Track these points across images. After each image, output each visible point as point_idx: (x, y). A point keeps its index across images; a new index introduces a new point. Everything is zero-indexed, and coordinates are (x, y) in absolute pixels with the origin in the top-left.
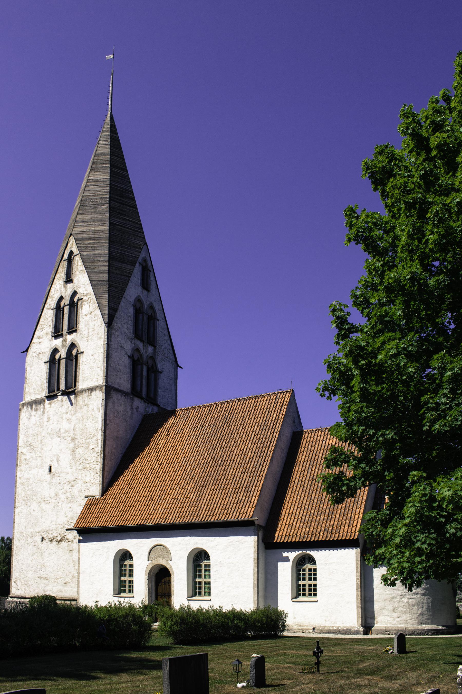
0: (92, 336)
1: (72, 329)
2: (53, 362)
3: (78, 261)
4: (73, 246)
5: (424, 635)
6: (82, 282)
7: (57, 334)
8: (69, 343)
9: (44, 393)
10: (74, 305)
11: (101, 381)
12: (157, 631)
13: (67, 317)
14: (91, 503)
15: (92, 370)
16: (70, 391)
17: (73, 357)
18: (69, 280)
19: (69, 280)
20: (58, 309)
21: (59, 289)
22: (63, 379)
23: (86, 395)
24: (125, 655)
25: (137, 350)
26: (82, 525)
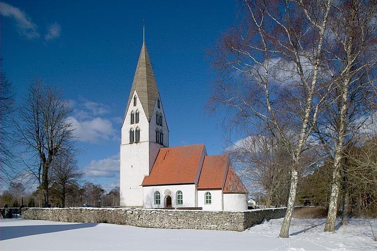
0: (144, 125)
1: (137, 122)
2: (131, 133)
3: (138, 99)
4: (135, 93)
5: (71, 222)
6: (139, 107)
7: (132, 123)
8: (136, 127)
9: (129, 142)
10: (137, 114)
11: (148, 139)
12: (348, 109)
13: (135, 118)
14: (146, 177)
15: (145, 135)
16: (138, 141)
17: (138, 132)
18: (135, 105)
19: (135, 105)
20: (132, 115)
21: (131, 108)
22: (135, 137)
23: (143, 143)
24: (144, 44)
25: (157, 128)
26: (144, 184)
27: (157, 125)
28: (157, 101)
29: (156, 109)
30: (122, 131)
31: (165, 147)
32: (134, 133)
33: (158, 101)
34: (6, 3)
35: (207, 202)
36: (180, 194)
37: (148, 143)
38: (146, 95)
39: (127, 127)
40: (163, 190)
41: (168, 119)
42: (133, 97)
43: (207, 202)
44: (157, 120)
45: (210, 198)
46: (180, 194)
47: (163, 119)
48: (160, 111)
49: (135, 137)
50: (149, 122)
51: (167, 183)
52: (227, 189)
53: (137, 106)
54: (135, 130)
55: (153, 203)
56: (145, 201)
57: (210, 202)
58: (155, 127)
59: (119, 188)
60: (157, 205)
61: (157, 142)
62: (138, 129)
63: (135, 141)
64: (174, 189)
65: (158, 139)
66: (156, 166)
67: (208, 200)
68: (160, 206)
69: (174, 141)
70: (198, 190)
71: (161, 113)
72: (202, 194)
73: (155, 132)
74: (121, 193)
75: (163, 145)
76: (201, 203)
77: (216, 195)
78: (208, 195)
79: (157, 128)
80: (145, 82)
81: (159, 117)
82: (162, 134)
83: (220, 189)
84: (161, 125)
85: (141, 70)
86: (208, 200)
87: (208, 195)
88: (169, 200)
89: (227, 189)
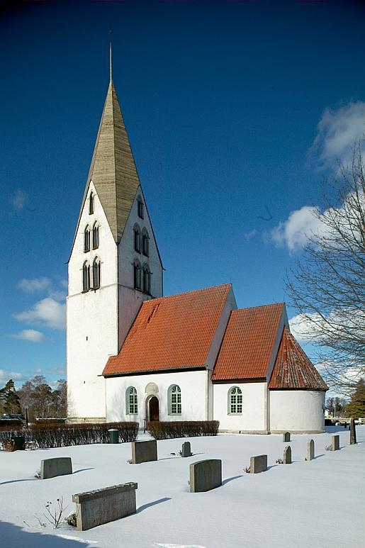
0: (108, 252)
1: (95, 247)
2: (85, 269)
3: (96, 200)
7: (87, 250)
10: (96, 231)
11: (115, 280)
13: (92, 240)
14: (112, 359)
15: (109, 274)
17: (97, 267)
18: (91, 212)
19: (91, 212)
21: (86, 220)
22: (92, 279)
24: (110, 92)
27: (136, 253)
28: (136, 203)
29: (134, 218)
30: (69, 268)
31: (153, 298)
32: (91, 269)
33: (140, 203)
34: (299, 209)
35: (233, 410)
36: (177, 393)
37: (115, 289)
38: (112, 191)
39: (78, 258)
40: (142, 384)
41: (160, 241)
42: (88, 196)
43: (233, 410)
44: (137, 244)
45: (240, 399)
46: (177, 393)
47: (151, 241)
48: (144, 224)
49: (92, 279)
50: (118, 244)
51: (149, 369)
52: (279, 378)
53: (96, 215)
54: (91, 265)
55: (125, 412)
56: (110, 408)
57: (240, 411)
58: (131, 256)
59: (66, 382)
60: (132, 416)
61: (136, 287)
62: (97, 261)
63: (92, 286)
64: (163, 382)
65: (138, 281)
66: (132, 336)
67: (236, 406)
68: (138, 417)
69: (178, 283)
70: (215, 382)
71: (145, 229)
72: (222, 391)
73: (132, 268)
74: (68, 393)
75: (150, 295)
76: (221, 414)
77: (253, 392)
78: (237, 394)
79: (137, 260)
80: (112, 162)
81: (140, 237)
82: (147, 272)
83: (262, 380)
84: (146, 255)
85: (106, 139)
86: (236, 406)
87: (237, 394)
88: (154, 404)
89: (279, 378)
